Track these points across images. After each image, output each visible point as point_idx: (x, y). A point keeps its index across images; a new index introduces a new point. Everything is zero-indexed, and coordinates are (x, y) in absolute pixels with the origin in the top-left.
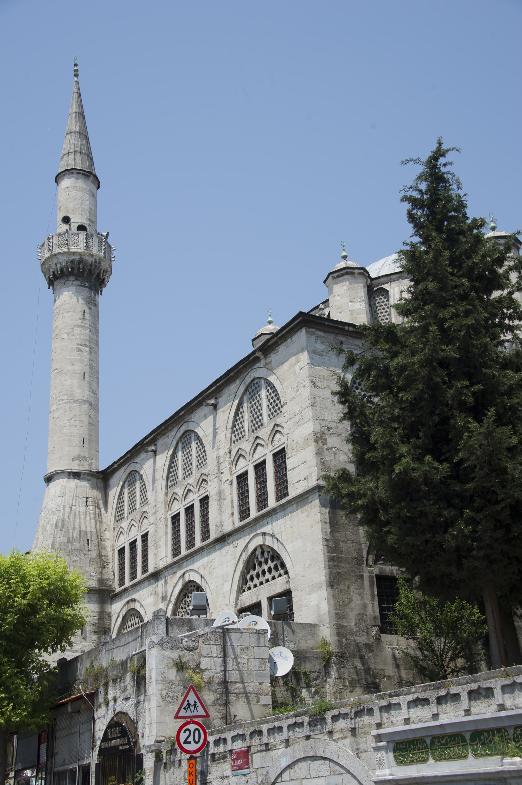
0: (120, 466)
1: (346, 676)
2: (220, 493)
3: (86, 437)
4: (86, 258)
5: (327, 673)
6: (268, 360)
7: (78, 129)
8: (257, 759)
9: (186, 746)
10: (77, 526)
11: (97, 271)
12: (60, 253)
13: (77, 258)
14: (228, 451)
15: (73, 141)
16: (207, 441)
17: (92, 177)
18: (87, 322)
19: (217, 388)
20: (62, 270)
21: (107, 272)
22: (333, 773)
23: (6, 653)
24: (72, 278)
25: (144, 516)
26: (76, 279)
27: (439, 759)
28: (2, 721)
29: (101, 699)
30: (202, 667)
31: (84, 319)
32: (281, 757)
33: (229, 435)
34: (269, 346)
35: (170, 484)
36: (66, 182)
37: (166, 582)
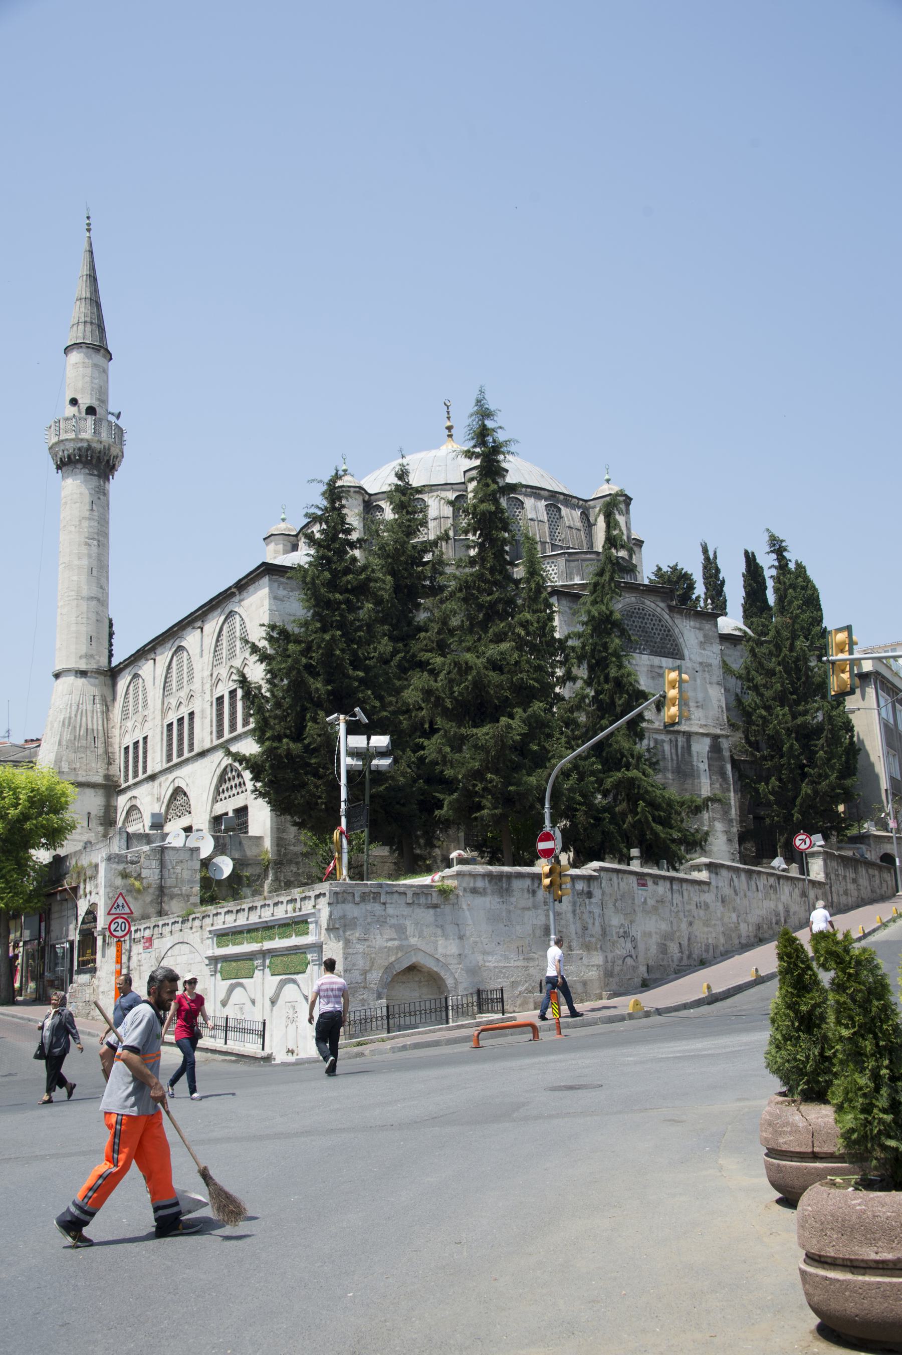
0: (126, 667)
1: (282, 878)
2: (203, 711)
3: (94, 635)
4: (94, 445)
5: (266, 876)
6: (242, 597)
7: (88, 295)
8: (156, 943)
9: (115, 933)
10: (84, 724)
11: (106, 458)
12: (67, 440)
13: (85, 445)
14: (209, 674)
15: (83, 309)
16: (195, 658)
17: (102, 351)
18: (95, 513)
19: (203, 612)
20: (69, 457)
21: (117, 457)
22: (191, 952)
23: (4, 852)
24: (80, 466)
25: (145, 719)
26: (84, 467)
27: (234, 944)
28: (2, 905)
29: (81, 892)
30: (143, 876)
31: (92, 510)
32: (168, 941)
33: (211, 659)
34: (242, 586)
35: (166, 693)
36: (75, 357)
37: (160, 784)
